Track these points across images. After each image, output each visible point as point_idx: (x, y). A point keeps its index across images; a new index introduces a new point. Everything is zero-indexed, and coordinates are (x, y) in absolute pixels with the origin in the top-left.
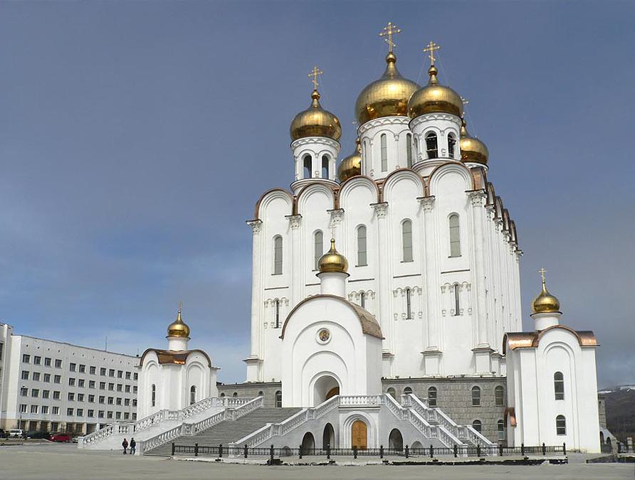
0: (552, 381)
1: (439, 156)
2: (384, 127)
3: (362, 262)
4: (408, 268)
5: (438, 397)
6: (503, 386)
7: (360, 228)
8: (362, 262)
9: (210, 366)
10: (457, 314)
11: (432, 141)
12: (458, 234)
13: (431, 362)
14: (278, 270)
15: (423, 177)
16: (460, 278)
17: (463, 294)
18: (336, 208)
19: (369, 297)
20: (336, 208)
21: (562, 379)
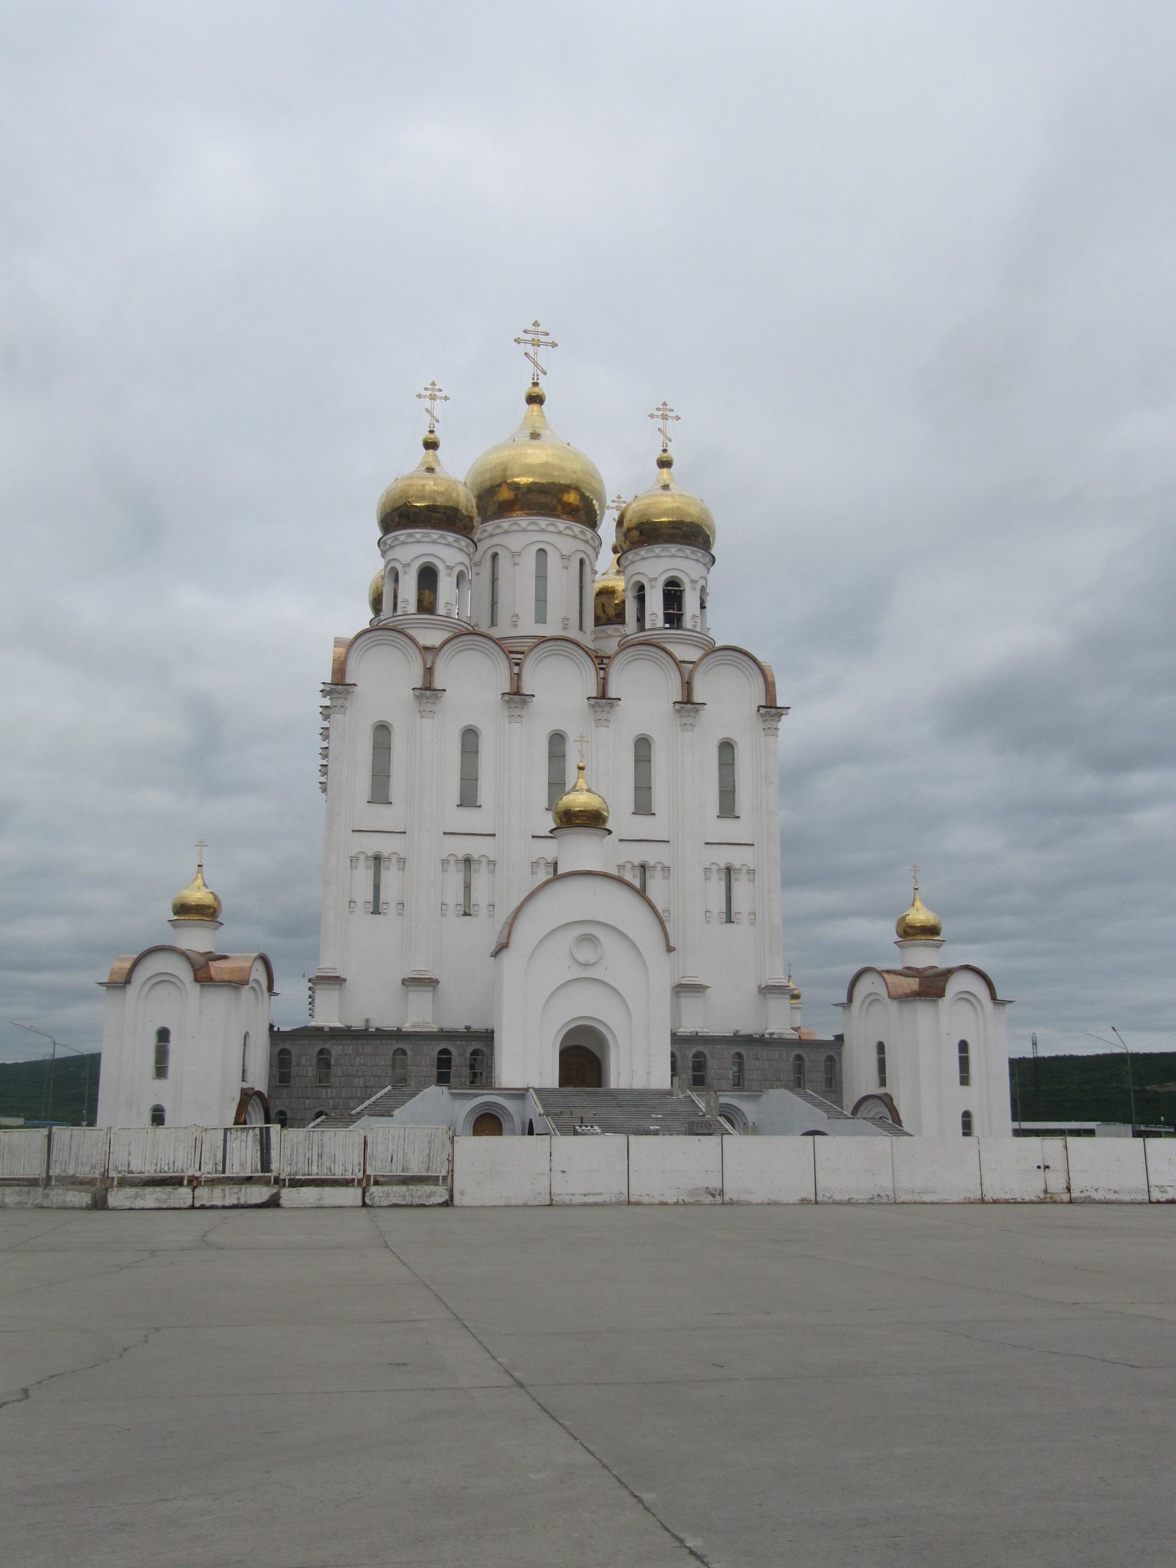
0: (152, 1041)
1: (646, 628)
2: (496, 540)
3: (643, 807)
4: (380, 816)
5: (453, 1068)
6: (836, 1057)
7: (380, 726)
8: (643, 807)
9: (993, 997)
10: (376, 911)
11: (428, 577)
12: (732, 776)
13: (689, 1002)
14: (380, 794)
15: (681, 662)
16: (737, 857)
17: (740, 887)
18: (603, 695)
19: (394, 866)
20: (603, 695)
21: (967, 1052)
